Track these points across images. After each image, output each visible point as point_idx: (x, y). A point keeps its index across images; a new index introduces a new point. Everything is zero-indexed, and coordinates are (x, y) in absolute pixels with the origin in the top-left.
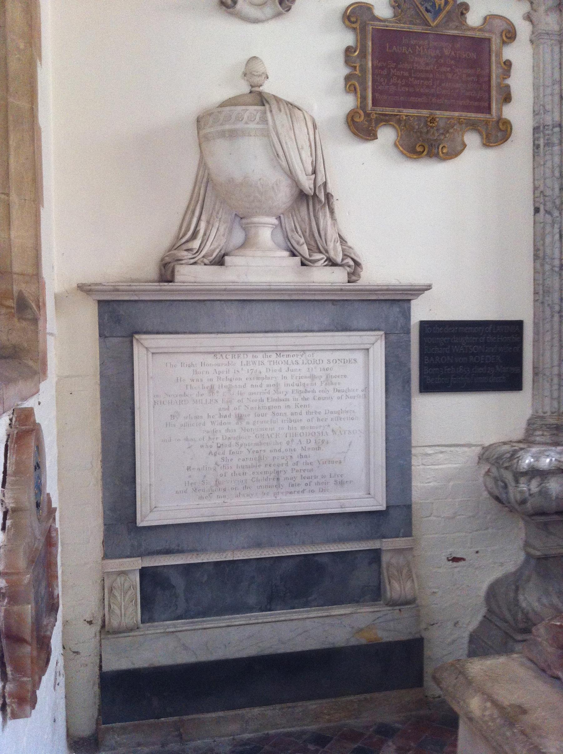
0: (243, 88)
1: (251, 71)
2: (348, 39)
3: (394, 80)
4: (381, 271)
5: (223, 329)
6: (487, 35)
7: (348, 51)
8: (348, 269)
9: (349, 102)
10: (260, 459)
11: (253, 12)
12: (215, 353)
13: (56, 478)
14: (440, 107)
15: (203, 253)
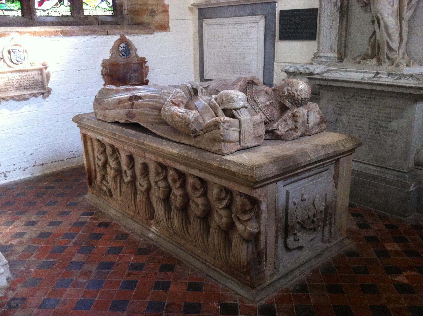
13: (340, 170)
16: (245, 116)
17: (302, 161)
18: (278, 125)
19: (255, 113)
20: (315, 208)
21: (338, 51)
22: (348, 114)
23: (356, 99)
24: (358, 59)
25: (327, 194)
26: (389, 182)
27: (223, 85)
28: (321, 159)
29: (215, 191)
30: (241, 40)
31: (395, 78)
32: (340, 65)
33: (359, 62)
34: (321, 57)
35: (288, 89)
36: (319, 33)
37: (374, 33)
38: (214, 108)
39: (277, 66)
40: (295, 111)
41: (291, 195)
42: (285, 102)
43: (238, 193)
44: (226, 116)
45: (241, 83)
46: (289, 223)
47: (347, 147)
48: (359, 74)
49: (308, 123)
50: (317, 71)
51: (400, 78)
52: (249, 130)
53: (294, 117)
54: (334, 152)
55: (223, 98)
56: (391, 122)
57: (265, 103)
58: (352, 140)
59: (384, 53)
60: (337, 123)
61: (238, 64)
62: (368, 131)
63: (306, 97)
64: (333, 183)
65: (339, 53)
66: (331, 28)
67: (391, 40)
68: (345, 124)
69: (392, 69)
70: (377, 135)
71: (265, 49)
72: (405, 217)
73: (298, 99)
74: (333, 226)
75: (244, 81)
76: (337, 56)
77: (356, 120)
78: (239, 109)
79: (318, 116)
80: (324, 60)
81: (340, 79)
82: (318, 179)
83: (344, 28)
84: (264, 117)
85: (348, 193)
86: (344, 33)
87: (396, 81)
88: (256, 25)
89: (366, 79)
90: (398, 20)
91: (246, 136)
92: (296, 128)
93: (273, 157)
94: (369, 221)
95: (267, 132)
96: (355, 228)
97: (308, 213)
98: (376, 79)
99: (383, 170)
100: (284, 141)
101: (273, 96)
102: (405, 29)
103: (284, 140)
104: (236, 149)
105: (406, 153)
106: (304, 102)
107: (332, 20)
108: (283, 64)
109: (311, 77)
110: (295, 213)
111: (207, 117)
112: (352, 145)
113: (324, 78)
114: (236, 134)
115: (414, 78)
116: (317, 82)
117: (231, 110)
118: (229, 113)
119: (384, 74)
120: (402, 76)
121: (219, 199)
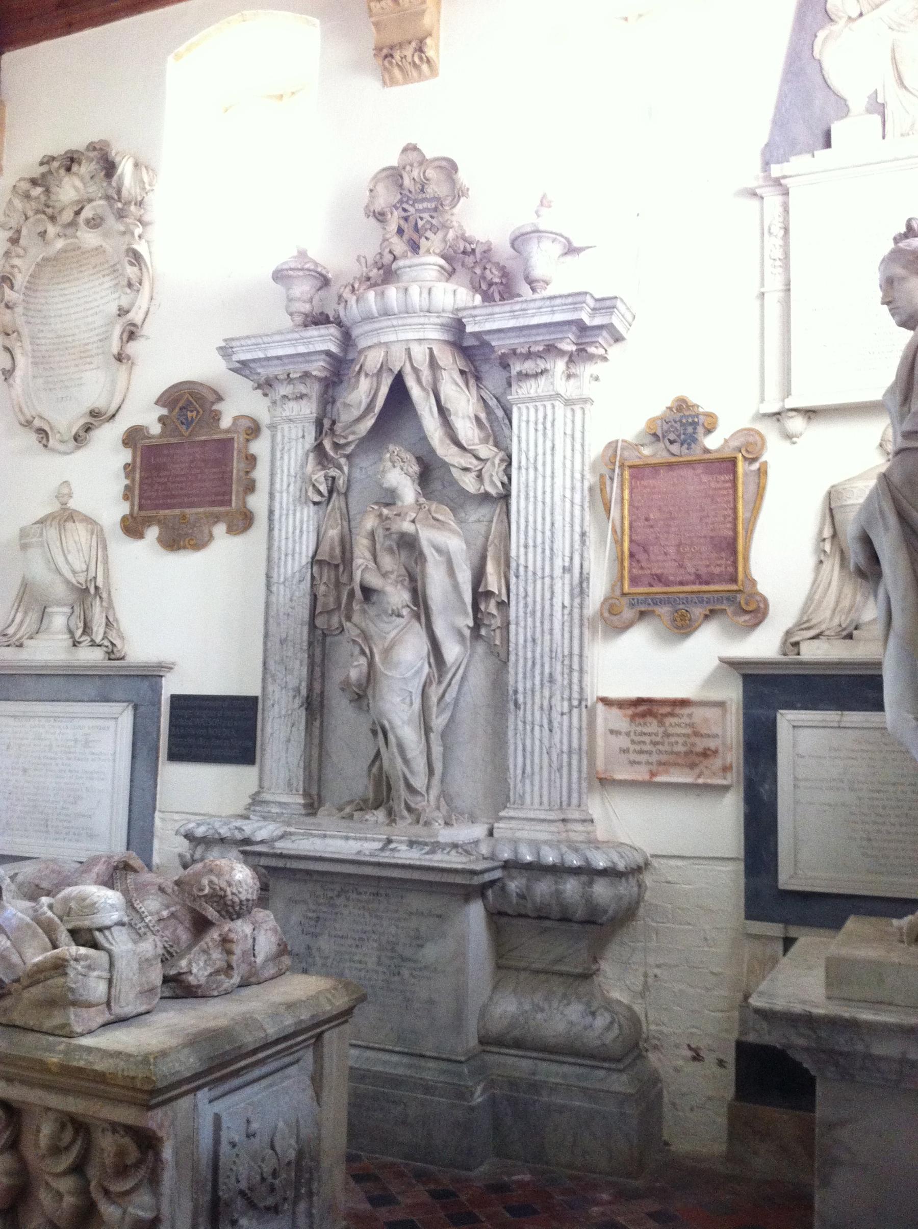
0: (55, 507)
1: (63, 494)
2: (126, 456)
3: (156, 487)
4: (140, 649)
5: (24, 698)
6: (229, 435)
7: (126, 466)
8: (105, 649)
9: (124, 508)
10: (35, 807)
11: (62, 447)
12: (15, 717)
14: (191, 505)
15: (18, 637)
16: (121, 943)
17: (250, 1039)
18: (190, 964)
19: (137, 937)
20: (277, 1154)
21: (304, 790)
22: (333, 933)
23: (348, 899)
24: (348, 810)
25: (302, 1122)
26: (428, 1089)
27: (53, 871)
28: (286, 1033)
29: (47, 1130)
30: (72, 756)
31: (424, 852)
32: (313, 824)
33: (351, 817)
34: (267, 803)
35: (211, 882)
36: (263, 750)
37: (378, 755)
38: (49, 929)
39: (163, 820)
40: (226, 929)
41: (226, 1122)
42: (205, 909)
43: (106, 1125)
44: (78, 944)
45: (100, 868)
46: (221, 1193)
47: (337, 1004)
48: (351, 843)
49: (254, 956)
50: (261, 835)
51: (432, 852)
52: (131, 974)
53: (225, 941)
54: (313, 1016)
55: (73, 904)
56: (422, 946)
57: (157, 913)
58: (347, 990)
59: (399, 797)
60: (310, 955)
61: (60, 814)
62: (377, 972)
63: (249, 897)
64: (310, 1092)
65: (306, 794)
66: (289, 741)
67: (412, 772)
68: (327, 958)
69: (419, 831)
70: (396, 978)
71: (132, 781)
72: (469, 1169)
73: (234, 903)
74: (315, 1198)
75: (108, 862)
76: (303, 802)
77: (350, 946)
78: (108, 928)
79: (274, 939)
80: (275, 810)
81: (312, 854)
82: (282, 1082)
83: (316, 741)
84: (160, 945)
85: (344, 1130)
86: (315, 752)
87: (427, 857)
88: (111, 723)
89: (367, 853)
90: (423, 732)
91: (123, 990)
92: (230, 967)
93: (188, 1035)
94: (394, 1188)
95: (166, 980)
96: (366, 1206)
97: (260, 1167)
98: (387, 853)
99: (415, 1061)
100: (202, 1000)
101: (177, 896)
102: (437, 750)
103: (203, 997)
104: (100, 1020)
105: (459, 1016)
106: (244, 907)
107: (290, 725)
108: (176, 817)
109: (248, 848)
110: (234, 1168)
111: (31, 950)
112: (346, 999)
113: (279, 851)
114: (102, 987)
115: (460, 850)
116: (264, 861)
117: (90, 930)
118: (84, 937)
119: (401, 842)
120: (436, 847)
121: (56, 1150)
